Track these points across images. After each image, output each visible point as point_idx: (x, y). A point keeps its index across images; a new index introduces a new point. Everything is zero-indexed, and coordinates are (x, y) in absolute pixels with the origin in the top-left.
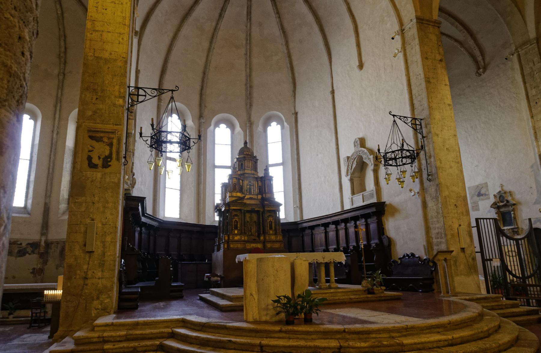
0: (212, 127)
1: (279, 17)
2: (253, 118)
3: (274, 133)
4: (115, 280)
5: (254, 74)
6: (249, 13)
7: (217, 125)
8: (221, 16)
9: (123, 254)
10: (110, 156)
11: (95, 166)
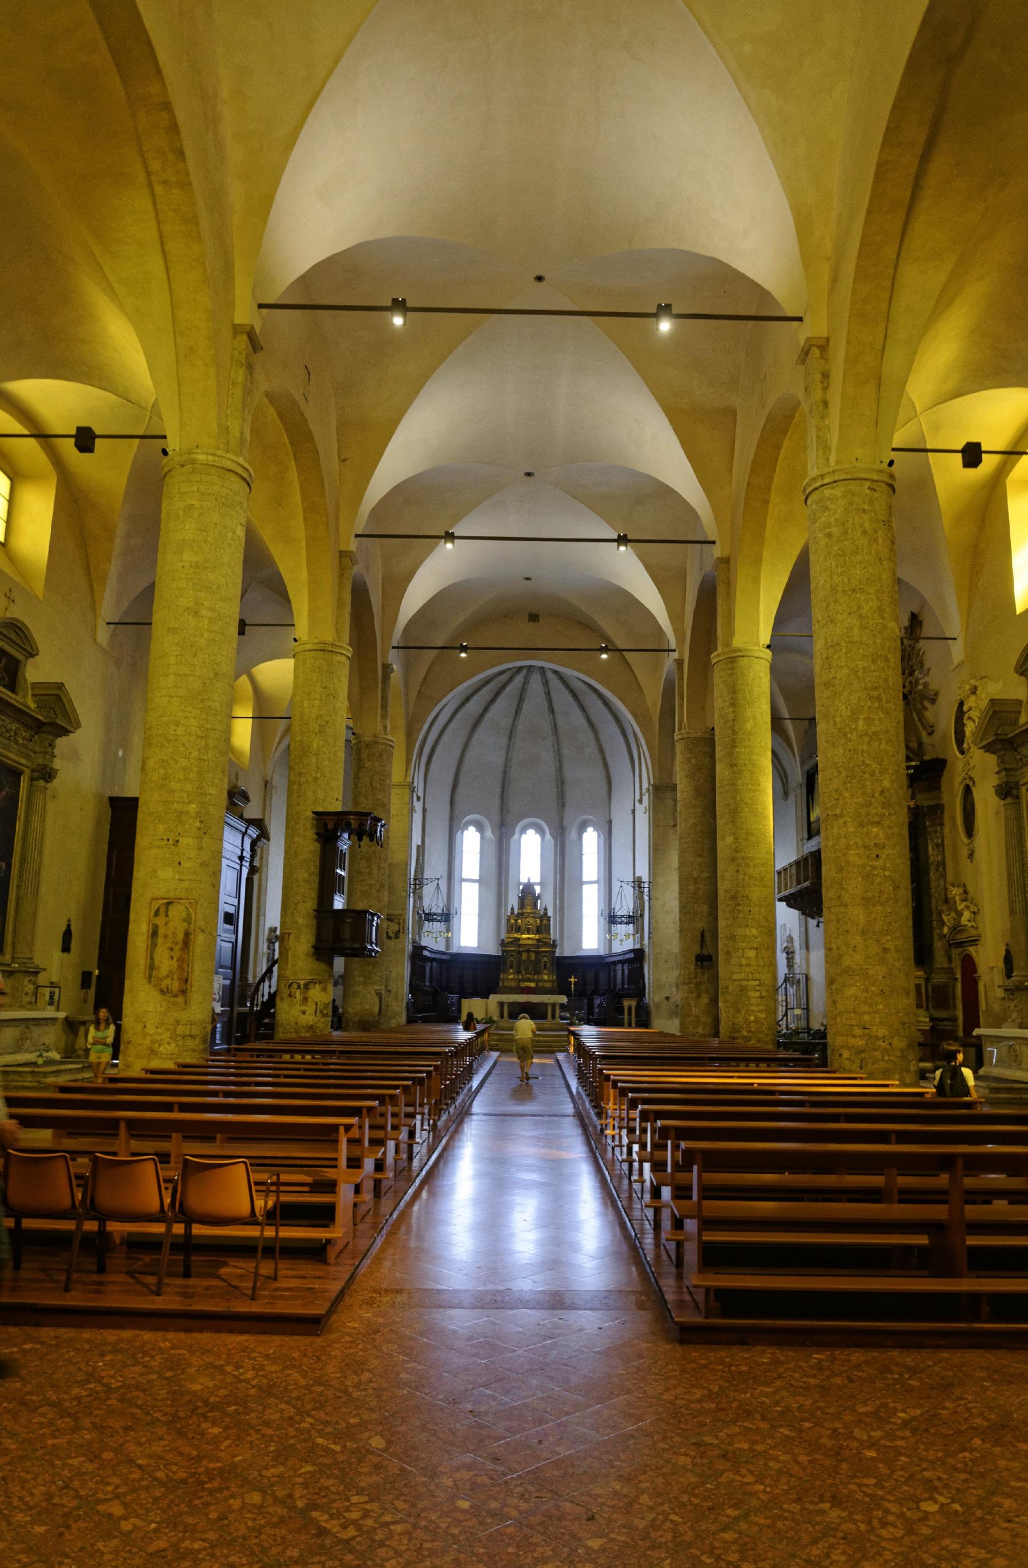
0: (516, 836)
2: (566, 823)
3: (591, 839)
4: (404, 1007)
5: (565, 767)
7: (523, 831)
10: (399, 931)
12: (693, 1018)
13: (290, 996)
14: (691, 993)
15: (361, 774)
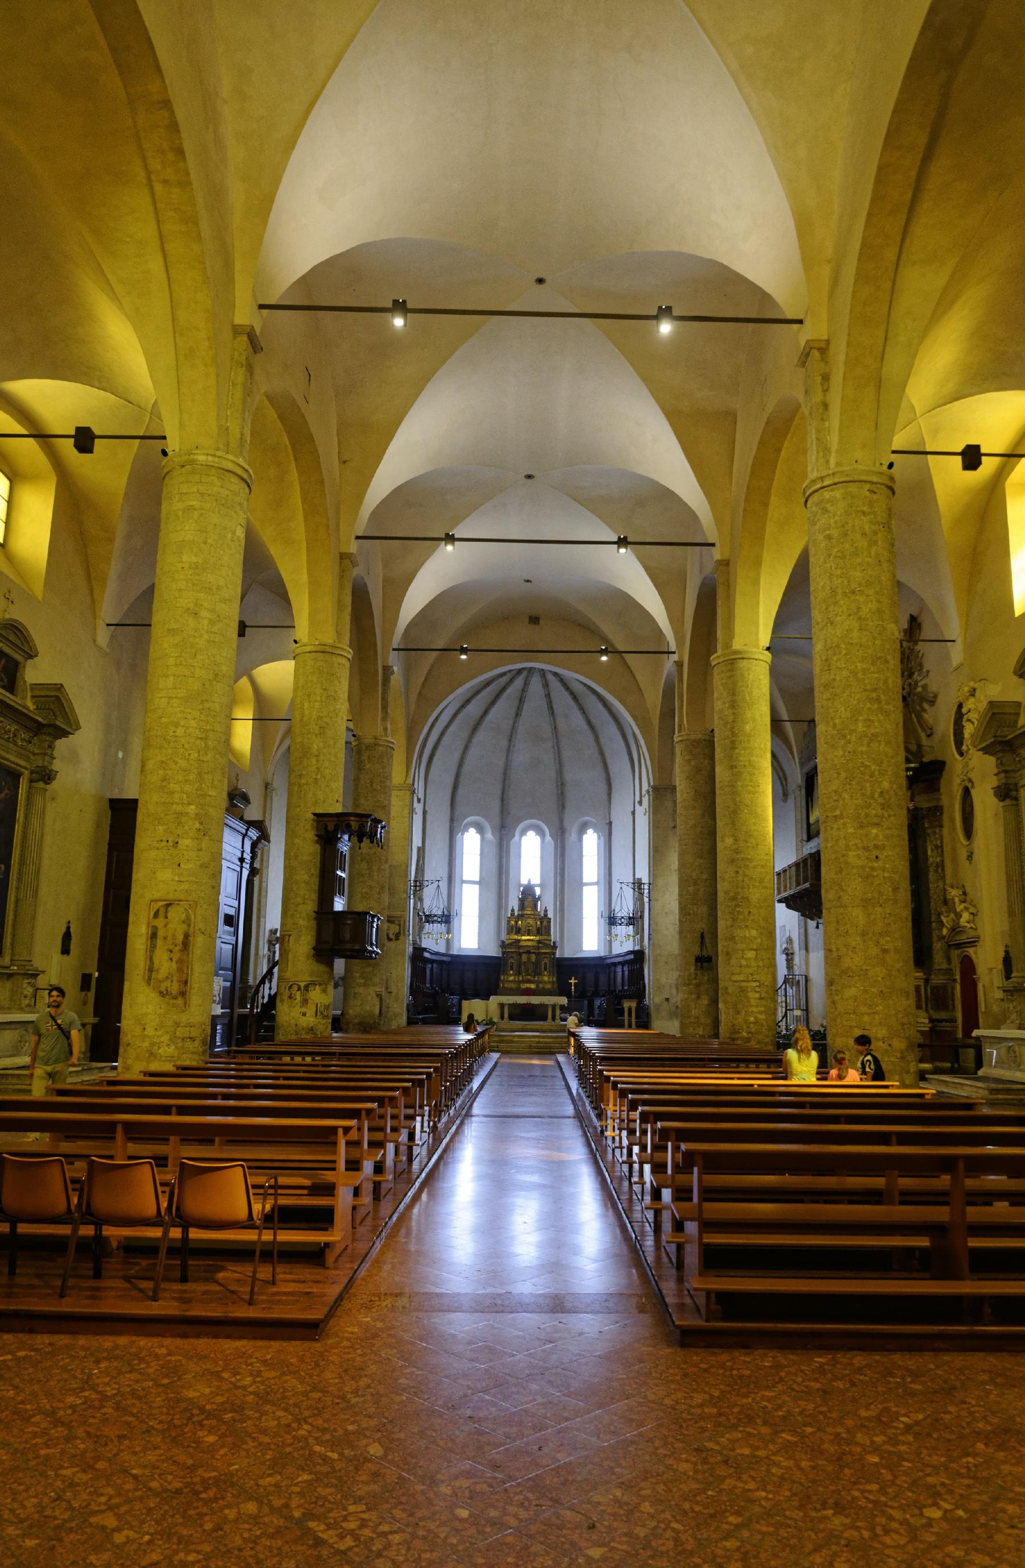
0: (517, 837)
1: (584, 713)
3: (591, 841)
6: (551, 708)
7: (523, 833)
8: (517, 715)
9: (413, 990)
11: (390, 940)
12: (692, 1019)
13: (290, 997)
14: (691, 994)
15: (362, 776)
